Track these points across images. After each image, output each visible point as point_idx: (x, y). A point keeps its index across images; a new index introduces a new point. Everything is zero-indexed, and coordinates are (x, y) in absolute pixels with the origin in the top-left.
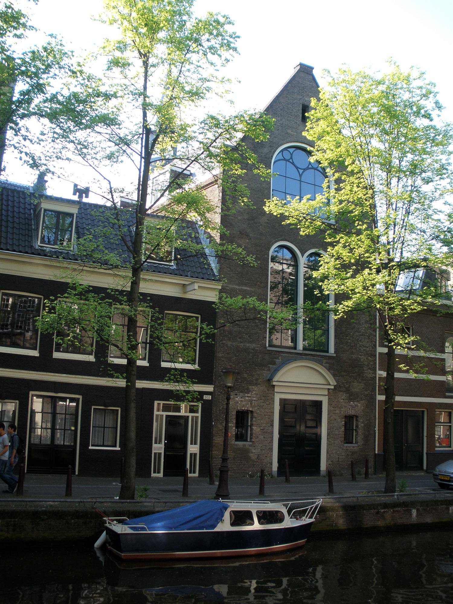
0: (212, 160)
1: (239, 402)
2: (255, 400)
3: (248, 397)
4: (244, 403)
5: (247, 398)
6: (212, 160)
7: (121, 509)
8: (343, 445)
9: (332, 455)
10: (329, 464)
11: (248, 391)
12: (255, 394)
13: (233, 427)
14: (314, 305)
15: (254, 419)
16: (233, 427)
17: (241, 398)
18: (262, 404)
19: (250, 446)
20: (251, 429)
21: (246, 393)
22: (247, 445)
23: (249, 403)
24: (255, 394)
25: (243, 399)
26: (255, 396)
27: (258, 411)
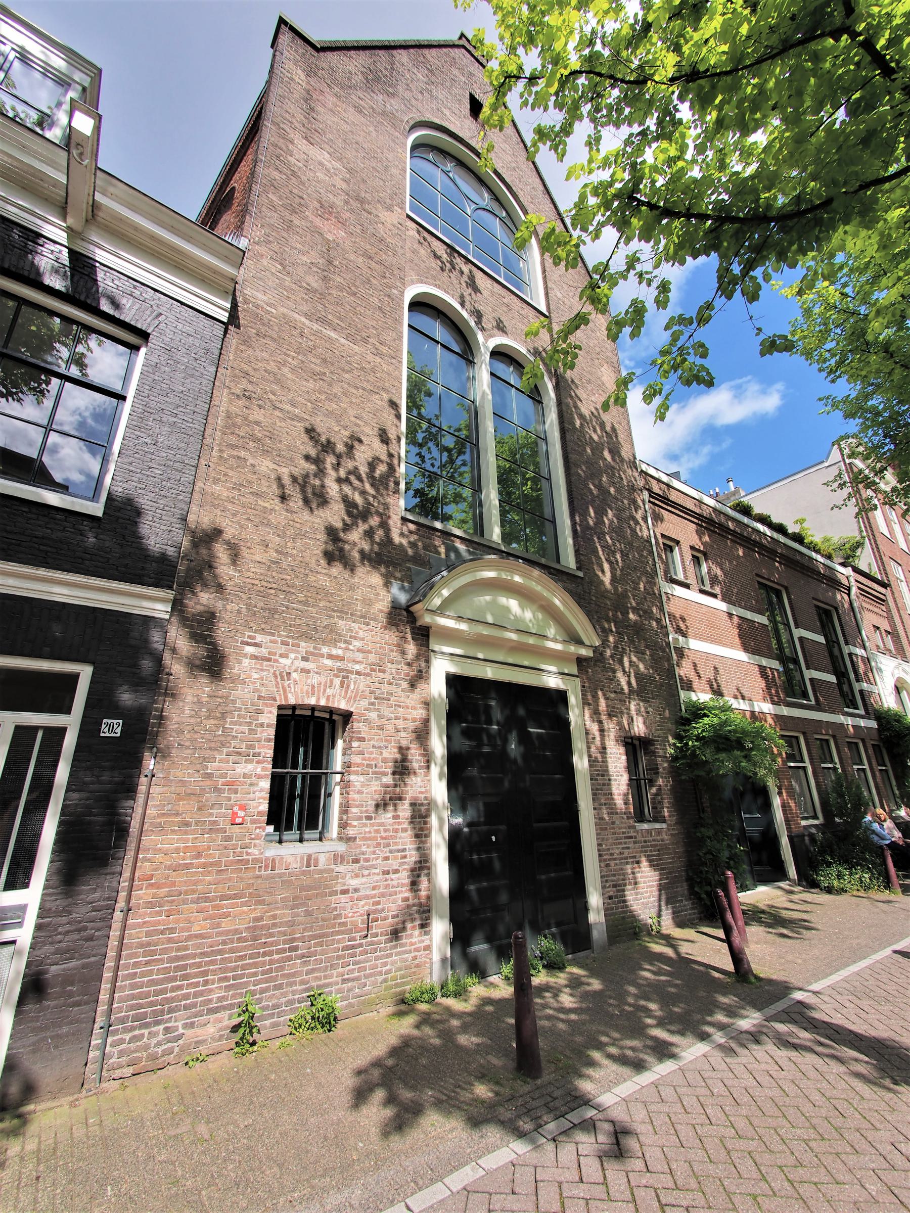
0: (423, 796)
1: (295, 675)
2: (358, 673)
3: (330, 657)
4: (315, 679)
5: (328, 662)
6: (423, 796)
7: (143, 780)
8: (634, 827)
9: (612, 863)
10: (610, 898)
11: (333, 637)
12: (359, 650)
13: (259, 777)
14: (867, 24)
15: (355, 744)
16: (259, 777)
17: (305, 659)
18: (386, 688)
19: (339, 859)
20: (346, 785)
21: (324, 642)
22: (322, 859)
23: (337, 682)
24: (359, 650)
25: (310, 666)
26: (359, 656)
27: (373, 715)
